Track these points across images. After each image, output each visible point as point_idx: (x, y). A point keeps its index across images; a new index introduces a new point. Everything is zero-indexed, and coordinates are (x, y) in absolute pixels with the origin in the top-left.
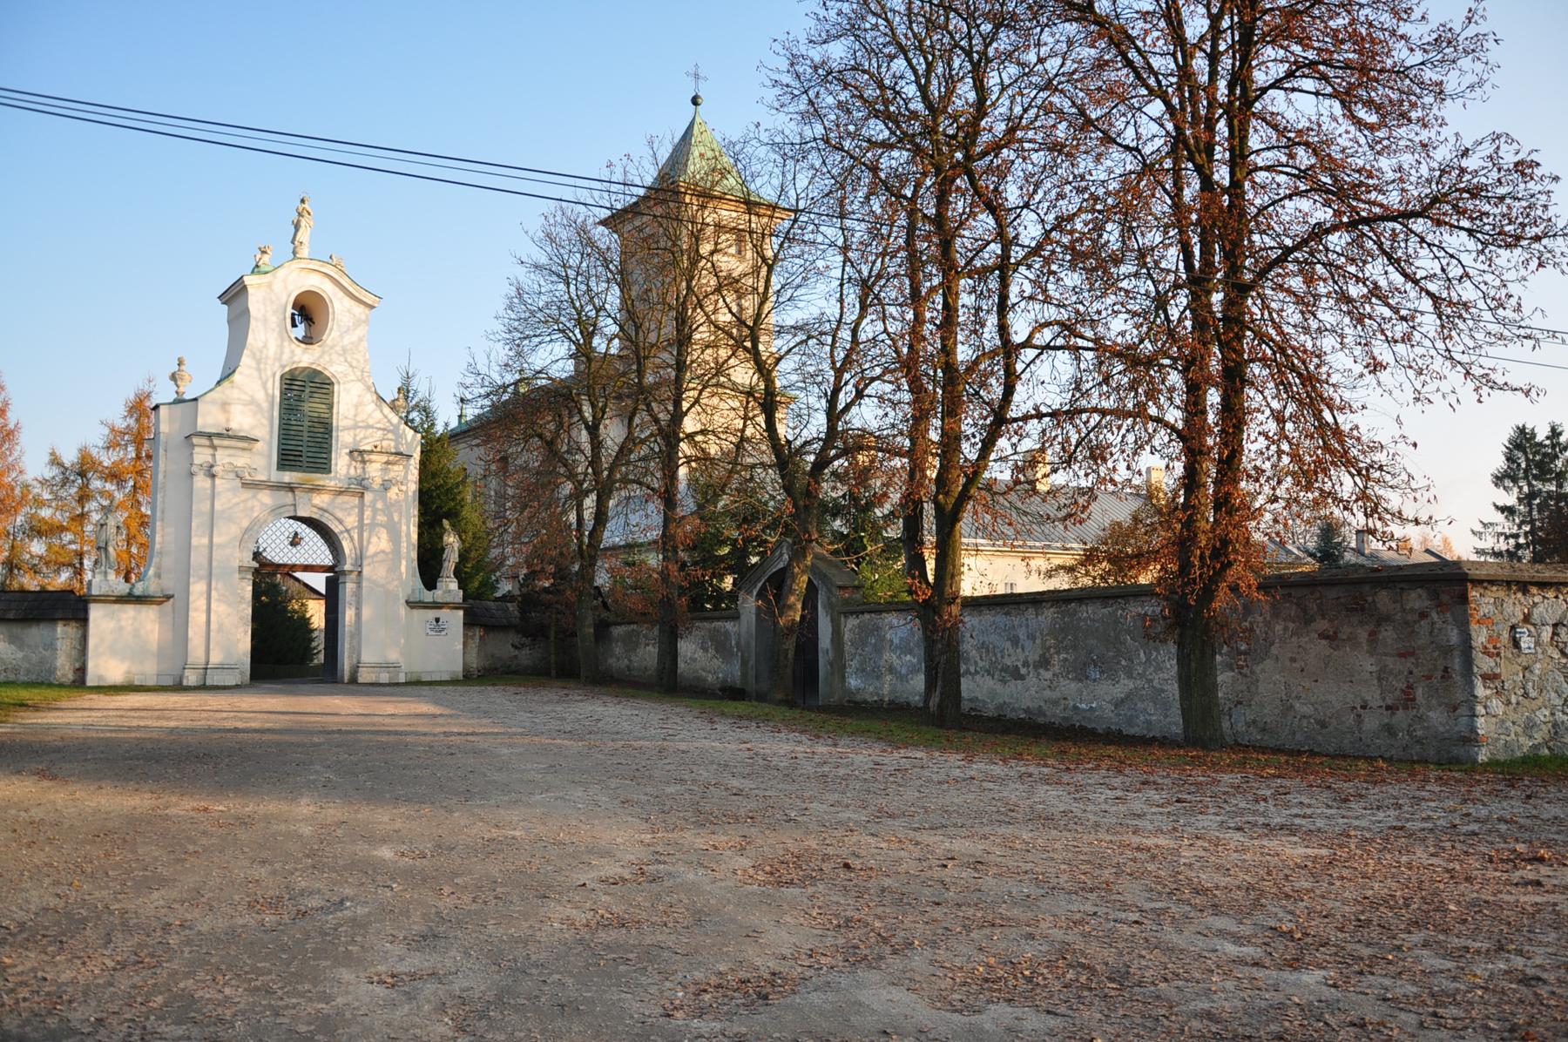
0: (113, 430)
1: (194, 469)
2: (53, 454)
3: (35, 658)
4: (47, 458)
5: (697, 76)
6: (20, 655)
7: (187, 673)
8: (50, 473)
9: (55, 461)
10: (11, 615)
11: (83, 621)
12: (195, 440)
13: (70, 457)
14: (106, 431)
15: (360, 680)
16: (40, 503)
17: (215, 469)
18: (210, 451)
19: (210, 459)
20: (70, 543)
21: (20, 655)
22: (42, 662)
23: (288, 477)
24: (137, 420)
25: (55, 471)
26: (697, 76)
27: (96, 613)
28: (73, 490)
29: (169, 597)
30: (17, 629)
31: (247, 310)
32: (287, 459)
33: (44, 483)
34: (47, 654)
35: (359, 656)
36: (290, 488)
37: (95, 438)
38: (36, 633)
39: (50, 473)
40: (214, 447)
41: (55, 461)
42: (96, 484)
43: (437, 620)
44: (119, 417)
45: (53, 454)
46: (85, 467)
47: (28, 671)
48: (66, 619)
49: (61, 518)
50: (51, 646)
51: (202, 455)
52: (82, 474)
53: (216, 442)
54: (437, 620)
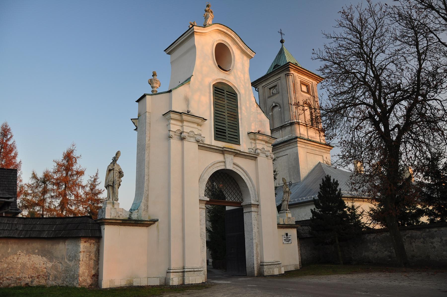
0: (58, 164)
1: (171, 133)
2: (34, 174)
3: (61, 267)
4: (31, 176)
5: (281, 33)
6: (50, 265)
7: (172, 276)
8: (31, 182)
9: (34, 176)
10: (45, 235)
11: (97, 237)
12: (173, 115)
13: (40, 175)
14: (56, 164)
15: (266, 274)
16: (26, 194)
17: (184, 134)
18: (180, 124)
19: (179, 128)
20: (38, 211)
21: (50, 265)
22: (67, 270)
23: (221, 144)
24: (67, 161)
25: (34, 181)
26: (281, 33)
27: (108, 231)
28: (40, 189)
29: (154, 221)
30: (48, 246)
31: (194, 47)
32: (219, 134)
33: (29, 186)
34: (72, 264)
35: (262, 257)
36: (223, 151)
37: (51, 167)
38: (62, 248)
39: (31, 182)
40: (182, 121)
41: (34, 176)
42: (50, 187)
43: (287, 234)
44: (60, 158)
45: (34, 174)
46: (47, 178)
47: (56, 277)
48: (87, 237)
49: (35, 200)
50: (75, 258)
51: (175, 126)
52: (44, 182)
53: (185, 117)
54: (287, 234)
